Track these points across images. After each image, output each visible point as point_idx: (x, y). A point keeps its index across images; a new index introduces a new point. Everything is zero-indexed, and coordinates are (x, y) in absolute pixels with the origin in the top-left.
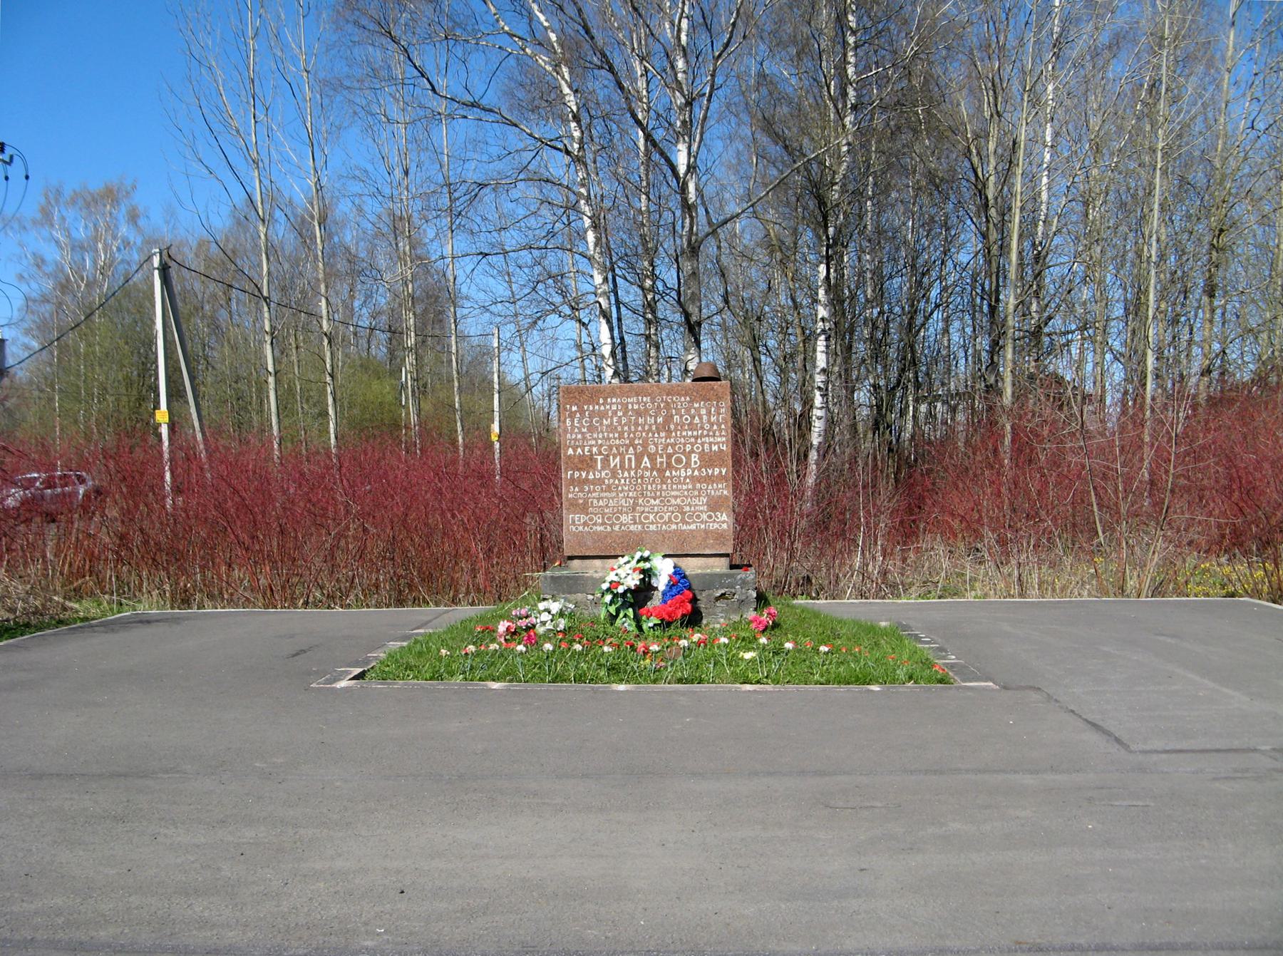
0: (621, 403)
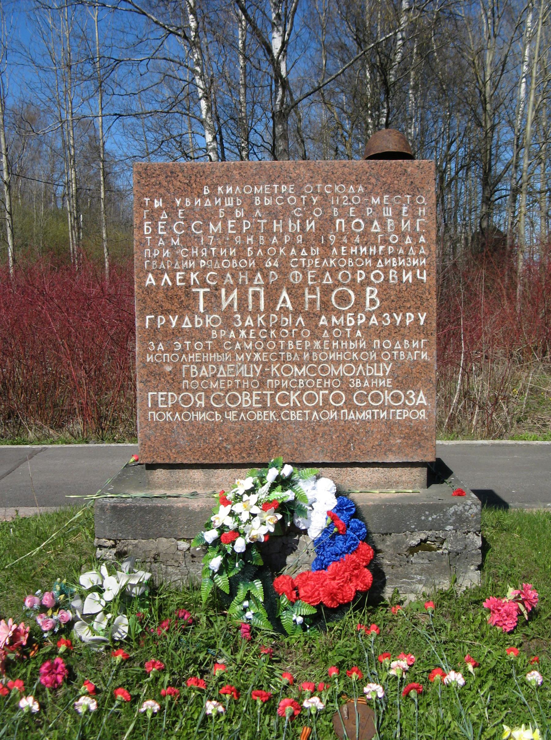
0: (242, 196)
